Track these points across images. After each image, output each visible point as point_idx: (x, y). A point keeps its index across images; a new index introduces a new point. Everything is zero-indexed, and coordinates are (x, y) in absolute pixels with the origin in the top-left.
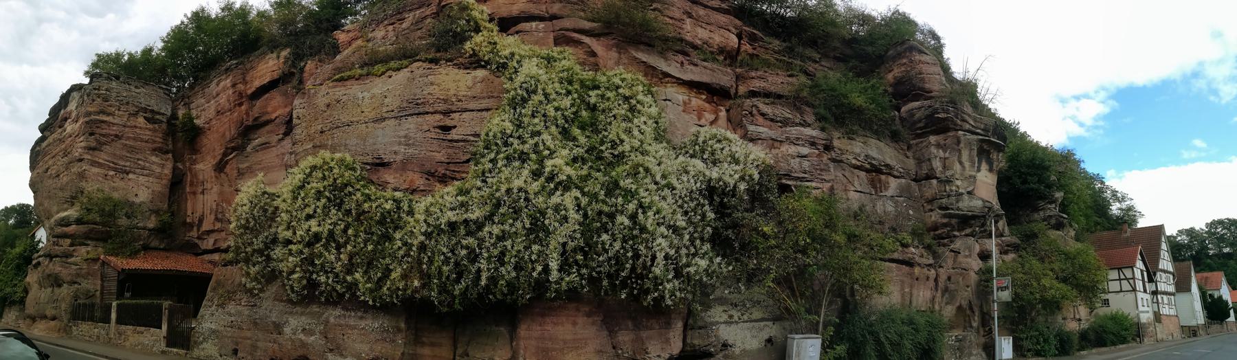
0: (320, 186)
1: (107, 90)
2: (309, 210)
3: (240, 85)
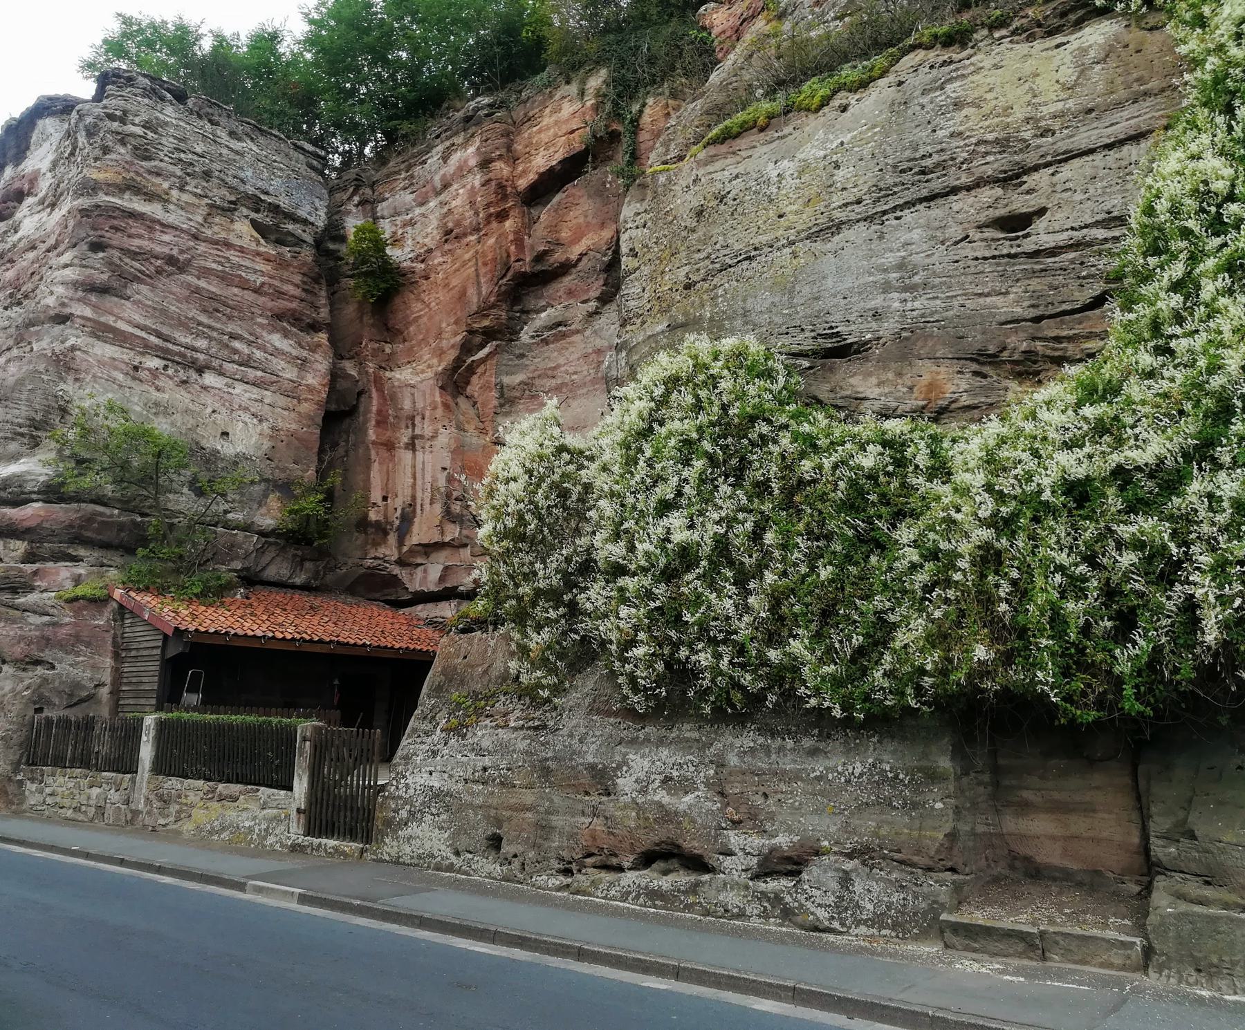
0: (688, 427)
1: (147, 125)
2: (666, 491)
3: (499, 165)
